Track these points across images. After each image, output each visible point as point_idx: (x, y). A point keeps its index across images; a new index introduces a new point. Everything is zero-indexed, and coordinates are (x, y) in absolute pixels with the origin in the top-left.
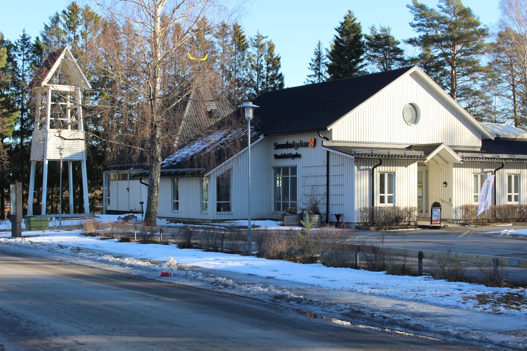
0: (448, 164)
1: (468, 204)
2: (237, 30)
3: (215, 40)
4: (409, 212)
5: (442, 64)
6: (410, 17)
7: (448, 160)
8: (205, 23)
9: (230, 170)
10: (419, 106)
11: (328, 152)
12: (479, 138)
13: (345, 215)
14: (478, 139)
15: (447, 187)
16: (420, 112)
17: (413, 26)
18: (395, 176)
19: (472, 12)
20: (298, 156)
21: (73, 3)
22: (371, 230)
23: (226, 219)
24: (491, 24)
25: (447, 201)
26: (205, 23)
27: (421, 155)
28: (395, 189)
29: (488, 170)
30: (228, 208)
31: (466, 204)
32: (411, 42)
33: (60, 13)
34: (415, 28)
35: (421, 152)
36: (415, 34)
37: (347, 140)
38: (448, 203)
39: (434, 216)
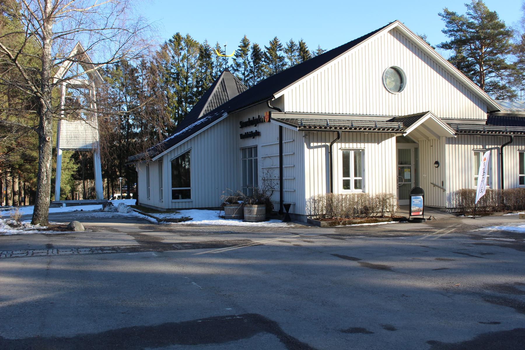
0: (440, 139)
1: (467, 188)
2: (302, 46)
3: (285, 55)
4: (383, 201)
5: (473, 64)
6: (442, 24)
7: (439, 134)
8: (276, 42)
9: (189, 152)
10: (405, 71)
11: (281, 128)
12: (484, 110)
13: (297, 204)
14: (482, 111)
15: (439, 167)
16: (406, 77)
17: (445, 32)
18: (364, 154)
19: (497, 15)
20: (257, 134)
21: (177, 33)
22: (322, 225)
23: (180, 207)
24: (513, 23)
25: (439, 185)
26: (276, 42)
27: (399, 127)
28: (364, 170)
29: (493, 146)
30: (186, 195)
31: (464, 188)
32: (445, 46)
33: (168, 42)
34: (447, 34)
35: (399, 123)
36: (448, 39)
37: (298, 111)
38: (440, 187)
39: (414, 205)
